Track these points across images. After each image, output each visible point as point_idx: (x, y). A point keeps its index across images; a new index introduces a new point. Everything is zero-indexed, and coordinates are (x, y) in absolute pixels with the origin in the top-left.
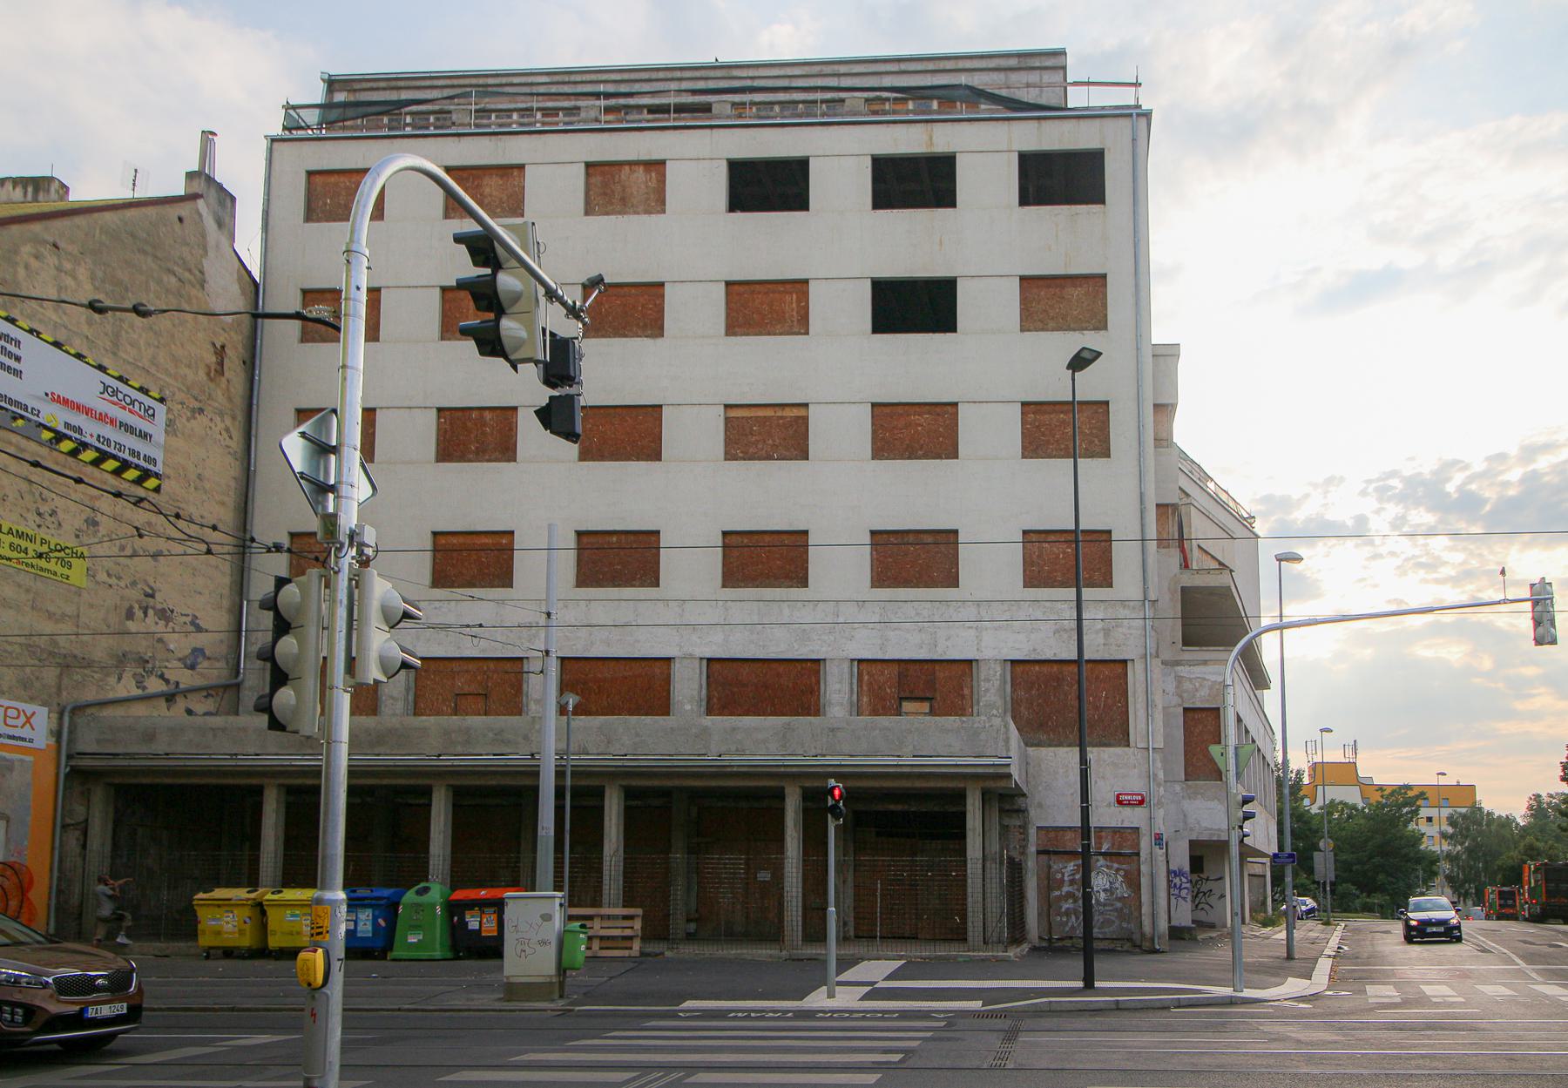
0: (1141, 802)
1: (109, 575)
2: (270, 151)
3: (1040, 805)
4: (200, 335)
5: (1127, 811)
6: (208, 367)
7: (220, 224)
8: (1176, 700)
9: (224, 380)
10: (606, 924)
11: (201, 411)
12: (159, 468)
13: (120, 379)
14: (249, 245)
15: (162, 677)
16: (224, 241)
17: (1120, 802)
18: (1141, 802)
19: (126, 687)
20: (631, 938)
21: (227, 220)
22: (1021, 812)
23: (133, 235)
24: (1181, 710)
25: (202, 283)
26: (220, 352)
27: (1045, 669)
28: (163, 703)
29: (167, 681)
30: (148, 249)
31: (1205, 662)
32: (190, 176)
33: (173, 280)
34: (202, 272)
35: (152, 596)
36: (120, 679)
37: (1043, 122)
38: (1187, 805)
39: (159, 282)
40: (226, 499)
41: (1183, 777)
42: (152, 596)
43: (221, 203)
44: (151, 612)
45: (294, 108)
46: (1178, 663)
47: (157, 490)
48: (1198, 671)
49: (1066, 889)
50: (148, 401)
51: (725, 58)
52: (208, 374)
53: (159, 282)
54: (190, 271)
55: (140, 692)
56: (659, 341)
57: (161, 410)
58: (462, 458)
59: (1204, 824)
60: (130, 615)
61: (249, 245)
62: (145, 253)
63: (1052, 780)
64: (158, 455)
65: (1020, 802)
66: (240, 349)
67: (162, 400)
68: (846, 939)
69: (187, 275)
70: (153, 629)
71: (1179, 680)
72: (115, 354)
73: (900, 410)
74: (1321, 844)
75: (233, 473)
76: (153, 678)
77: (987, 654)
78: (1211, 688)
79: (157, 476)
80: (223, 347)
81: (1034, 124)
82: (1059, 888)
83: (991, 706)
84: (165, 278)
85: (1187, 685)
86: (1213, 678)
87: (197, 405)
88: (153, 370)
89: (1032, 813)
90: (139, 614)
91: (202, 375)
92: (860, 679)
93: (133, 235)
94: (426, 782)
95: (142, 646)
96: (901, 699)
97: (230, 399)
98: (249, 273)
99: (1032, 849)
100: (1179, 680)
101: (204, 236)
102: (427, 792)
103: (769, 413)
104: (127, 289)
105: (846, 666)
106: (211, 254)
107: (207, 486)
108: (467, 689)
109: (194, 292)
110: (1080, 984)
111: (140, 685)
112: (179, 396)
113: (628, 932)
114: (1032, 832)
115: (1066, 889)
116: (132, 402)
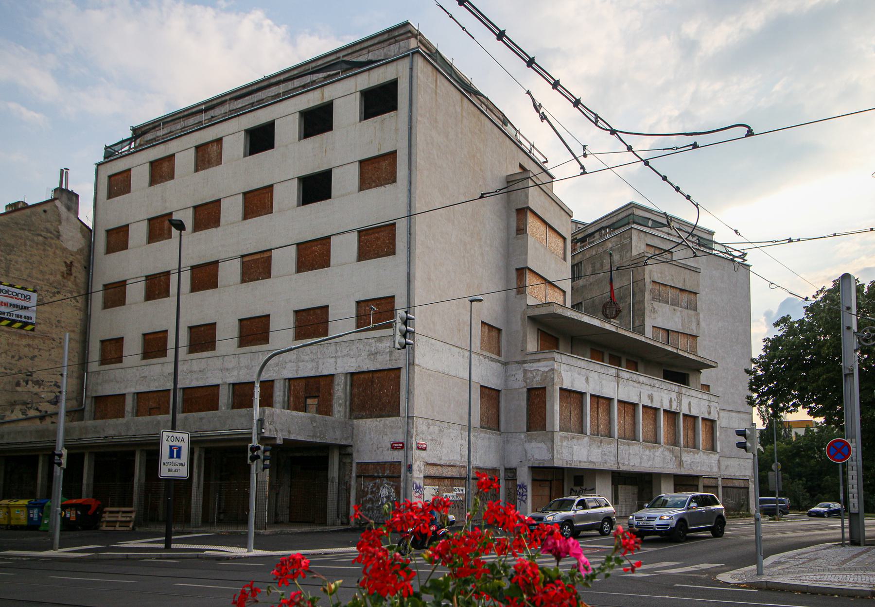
0: (402, 448)
1: (5, 369)
2: (97, 170)
3: (358, 451)
4: (58, 260)
5: (396, 453)
6: (63, 273)
7: (69, 209)
8: (523, 384)
9: (72, 278)
10: (124, 515)
11: (59, 293)
12: (34, 320)
13: (10, 286)
14: (86, 214)
15: (37, 409)
16: (72, 216)
17: (393, 448)
18: (402, 448)
19: (17, 414)
20: (129, 522)
21: (73, 206)
22: (350, 455)
23: (16, 223)
24: (525, 390)
25: (58, 237)
26: (69, 266)
27: (366, 376)
28: (38, 421)
29: (40, 411)
30: (26, 228)
31: (539, 360)
32: (56, 190)
33: (40, 238)
34: (58, 232)
35: (31, 375)
36: (12, 412)
37: (372, 72)
38: (527, 446)
39: (32, 240)
40: (76, 329)
41: (525, 430)
42: (31, 375)
43: (70, 199)
44: (30, 382)
45: (110, 147)
46: (524, 362)
47: (33, 330)
48: (535, 366)
49: (369, 496)
50: (26, 293)
51: (267, 75)
52: (63, 276)
53: (32, 240)
54: (51, 233)
55: (24, 417)
56: (219, 229)
57: (34, 296)
58: (154, 298)
59: (536, 457)
60: (18, 384)
61: (86, 214)
62: (24, 229)
63: (374, 438)
64: (33, 315)
65: (349, 450)
66: (83, 262)
67: (34, 291)
68: (276, 521)
69: (49, 235)
70: (32, 390)
71: (525, 372)
72: (7, 276)
73: (309, 245)
74: (773, 466)
75: (78, 317)
76: (32, 410)
77: (340, 370)
78: (542, 375)
79: (32, 324)
80: (71, 263)
81: (366, 74)
82: (366, 496)
83: (339, 398)
84: (36, 238)
85: (529, 375)
86: (543, 369)
87: (56, 290)
88: (29, 279)
89: (355, 455)
90: (23, 383)
91: (59, 277)
92: (289, 390)
93: (16, 223)
94: (131, 449)
95: (26, 398)
96: (306, 398)
97: (76, 285)
98: (87, 227)
99: (354, 475)
100: (525, 372)
101: (59, 215)
102: (133, 454)
103: (258, 256)
104: (13, 247)
105: (282, 382)
106: (64, 223)
107: (63, 325)
108: (154, 406)
109: (53, 242)
110: (163, 546)
111: (23, 413)
112: (45, 288)
113: (128, 519)
114: (354, 465)
115: (369, 496)
116: (17, 295)
